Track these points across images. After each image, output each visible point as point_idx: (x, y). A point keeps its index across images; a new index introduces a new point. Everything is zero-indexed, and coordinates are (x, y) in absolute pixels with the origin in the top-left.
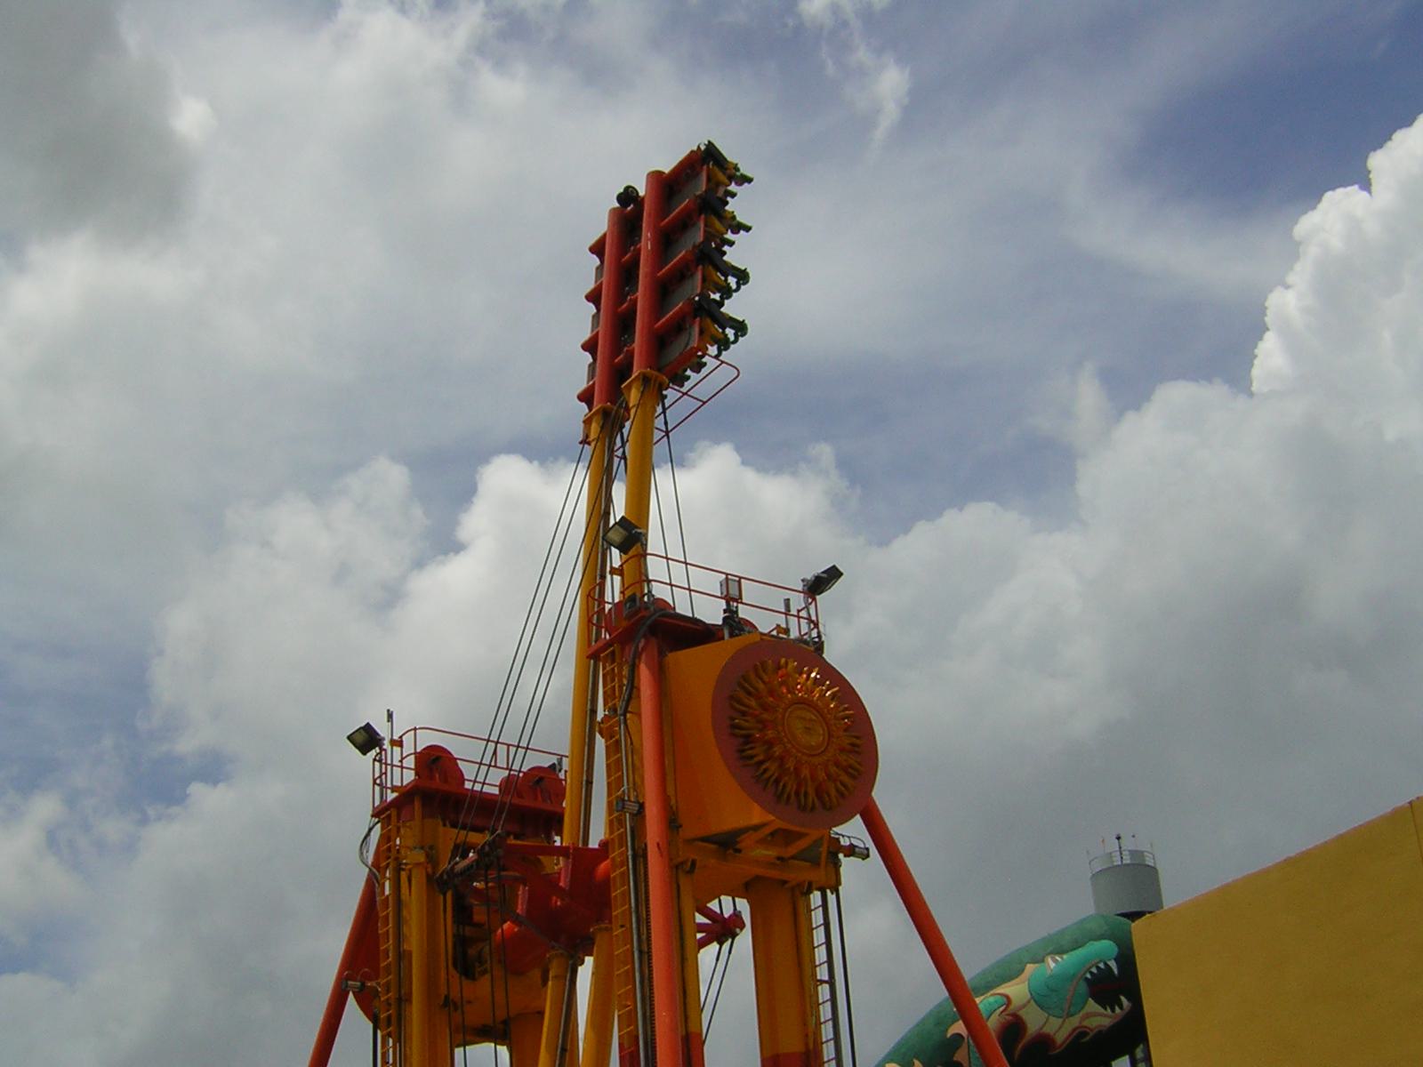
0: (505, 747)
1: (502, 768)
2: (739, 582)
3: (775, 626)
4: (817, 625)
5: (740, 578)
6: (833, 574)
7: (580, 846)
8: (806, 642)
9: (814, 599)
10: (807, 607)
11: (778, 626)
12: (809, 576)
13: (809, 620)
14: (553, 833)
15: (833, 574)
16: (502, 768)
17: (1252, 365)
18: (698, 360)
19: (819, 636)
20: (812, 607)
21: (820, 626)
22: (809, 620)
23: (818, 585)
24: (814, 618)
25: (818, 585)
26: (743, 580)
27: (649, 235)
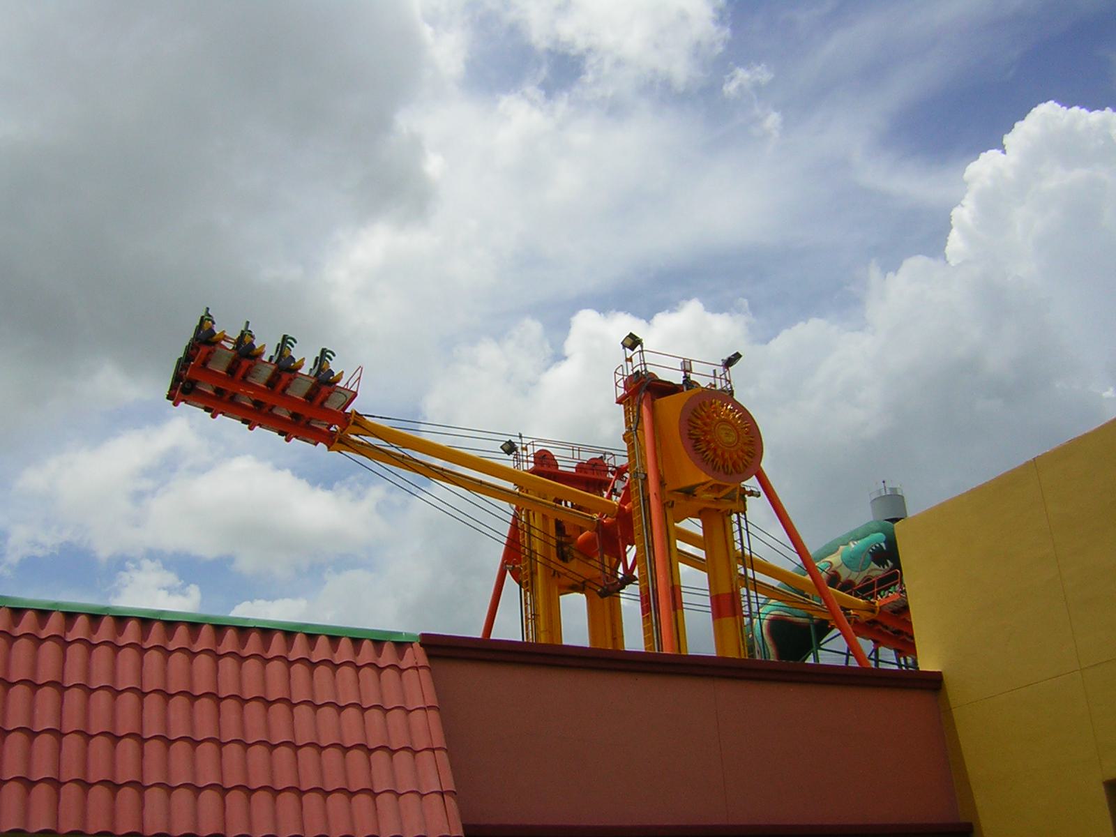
2: (690, 363)
4: (730, 382)
5: (691, 360)
8: (725, 391)
9: (728, 369)
19: (731, 387)
20: (727, 373)
22: (726, 380)
24: (728, 379)
26: (692, 362)
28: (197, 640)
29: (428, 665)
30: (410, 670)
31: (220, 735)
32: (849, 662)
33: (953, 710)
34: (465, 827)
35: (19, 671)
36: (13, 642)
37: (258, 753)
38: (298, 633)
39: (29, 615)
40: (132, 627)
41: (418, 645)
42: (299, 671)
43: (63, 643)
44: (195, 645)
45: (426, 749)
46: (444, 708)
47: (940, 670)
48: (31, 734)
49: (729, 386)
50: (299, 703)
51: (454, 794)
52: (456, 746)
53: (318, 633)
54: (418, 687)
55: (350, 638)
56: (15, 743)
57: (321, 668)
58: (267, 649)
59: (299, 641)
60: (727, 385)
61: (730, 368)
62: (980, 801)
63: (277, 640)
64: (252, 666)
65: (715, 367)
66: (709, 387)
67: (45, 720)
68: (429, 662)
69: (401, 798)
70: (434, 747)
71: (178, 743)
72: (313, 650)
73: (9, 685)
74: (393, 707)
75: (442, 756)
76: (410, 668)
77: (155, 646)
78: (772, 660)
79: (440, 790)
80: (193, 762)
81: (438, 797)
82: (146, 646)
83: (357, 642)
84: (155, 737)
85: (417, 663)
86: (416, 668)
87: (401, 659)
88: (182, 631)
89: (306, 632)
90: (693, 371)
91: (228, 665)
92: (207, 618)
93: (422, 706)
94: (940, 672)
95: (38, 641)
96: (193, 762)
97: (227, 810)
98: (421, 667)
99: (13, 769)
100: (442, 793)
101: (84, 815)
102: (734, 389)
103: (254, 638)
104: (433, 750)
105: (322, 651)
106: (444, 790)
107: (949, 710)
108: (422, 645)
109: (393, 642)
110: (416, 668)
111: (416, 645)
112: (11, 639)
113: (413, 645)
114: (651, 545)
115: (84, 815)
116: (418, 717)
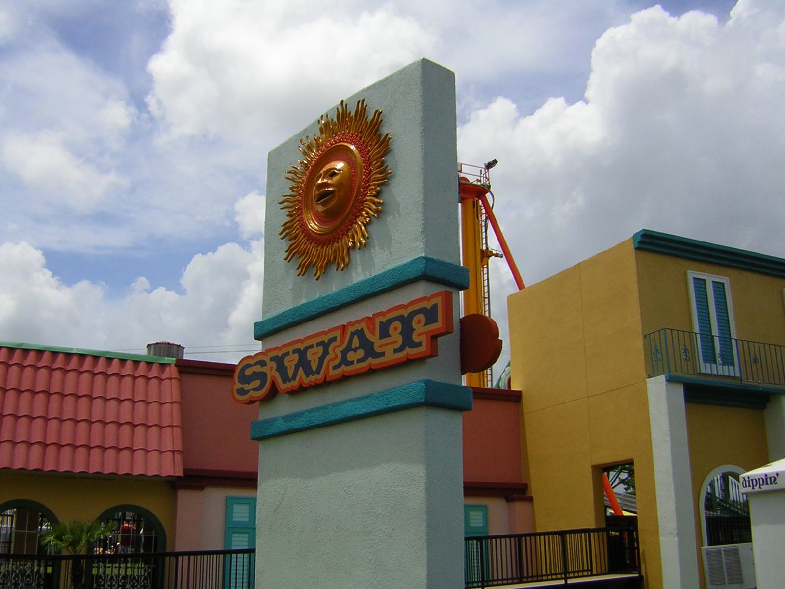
0: (741, 341)
1: (686, 332)
2: (461, 166)
3: (476, 179)
4: (488, 180)
5: (461, 164)
6: (495, 162)
7: (462, 265)
8: (484, 186)
9: (488, 171)
10: (485, 174)
11: (477, 179)
12: (487, 163)
13: (486, 178)
14: (666, 375)
15: (495, 162)
16: (686, 332)
17: (591, 57)
18: (621, 510)
19: (489, 183)
20: (487, 174)
21: (490, 180)
22: (486, 178)
23: (489, 166)
24: (487, 177)
25: (489, 166)
26: (462, 165)
27: (761, 389)
28: (41, 359)
29: (179, 378)
30: (167, 380)
31: (91, 417)
32: (512, 386)
33: (525, 415)
34: (185, 470)
35: (12, 383)
36: (23, 369)
37: (112, 428)
38: (127, 360)
39: (61, 356)
40: (32, 355)
41: (174, 365)
42: (99, 379)
43: (51, 370)
44: (40, 363)
45: (168, 426)
46: (183, 403)
47: (521, 390)
48: (17, 417)
49: (488, 182)
50: (138, 401)
51: (181, 452)
52: (186, 425)
53: (113, 357)
54: (171, 390)
55: (133, 361)
56: (8, 422)
57: (113, 378)
58: (82, 366)
59: (101, 362)
60: (486, 181)
61: (490, 170)
62: (532, 471)
63: (88, 361)
64: (71, 376)
65: (481, 169)
66: (476, 183)
67: (39, 411)
68: (179, 375)
69: (149, 453)
70: (173, 425)
71: (22, 418)
72: (136, 370)
73: (6, 391)
74: (152, 401)
75: (177, 431)
76: (166, 379)
77: (15, 364)
78: (463, 385)
79: (172, 449)
80: (30, 428)
81: (170, 454)
82: (11, 363)
83: (123, 361)
84: (24, 416)
85: (171, 376)
86: (170, 379)
87: (163, 373)
88: (32, 355)
89: (159, 362)
90: (463, 171)
91: (57, 375)
92: (48, 348)
93: (170, 401)
94: (520, 392)
95: (37, 369)
96: (30, 428)
97: (46, 456)
98: (173, 379)
99: (6, 436)
100: (173, 451)
101: (103, 463)
102: (491, 184)
103: (75, 360)
104: (172, 426)
105: (115, 368)
106: (175, 449)
107: (523, 415)
108: (176, 365)
109: (159, 363)
110: (170, 379)
111: (173, 366)
112: (7, 365)
113: (171, 365)
114: (688, 347)
115: (103, 463)
116: (167, 407)
